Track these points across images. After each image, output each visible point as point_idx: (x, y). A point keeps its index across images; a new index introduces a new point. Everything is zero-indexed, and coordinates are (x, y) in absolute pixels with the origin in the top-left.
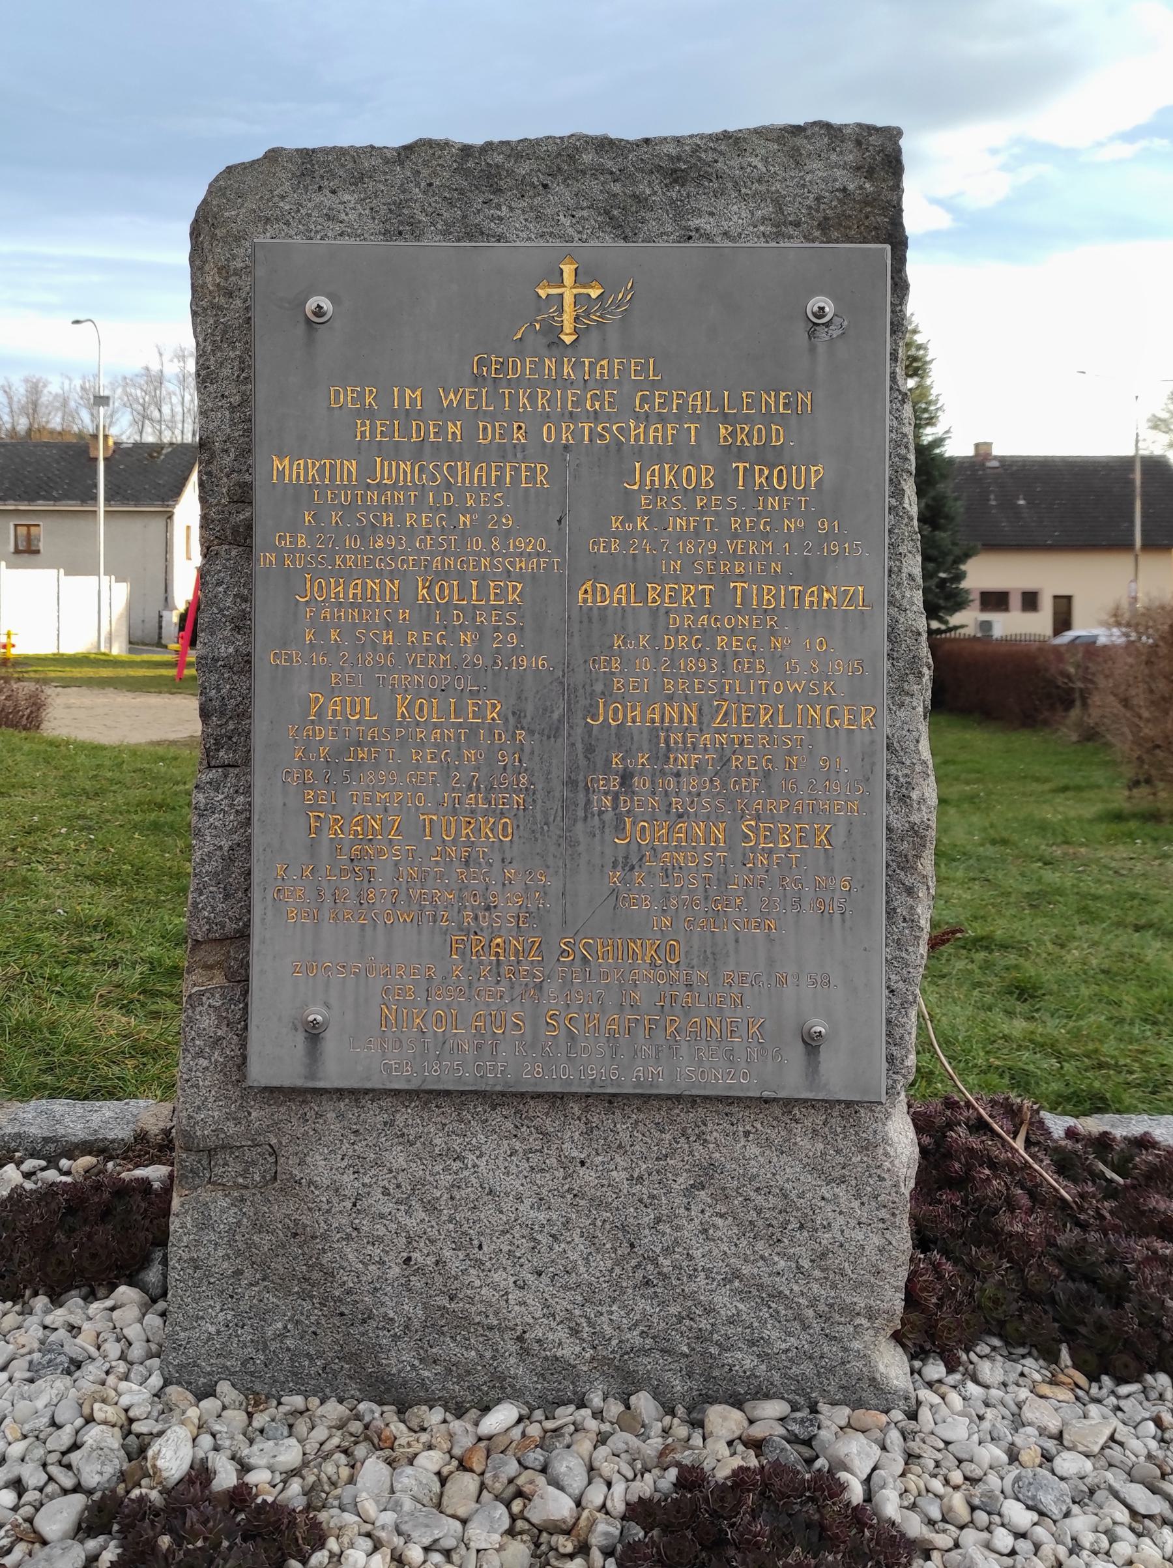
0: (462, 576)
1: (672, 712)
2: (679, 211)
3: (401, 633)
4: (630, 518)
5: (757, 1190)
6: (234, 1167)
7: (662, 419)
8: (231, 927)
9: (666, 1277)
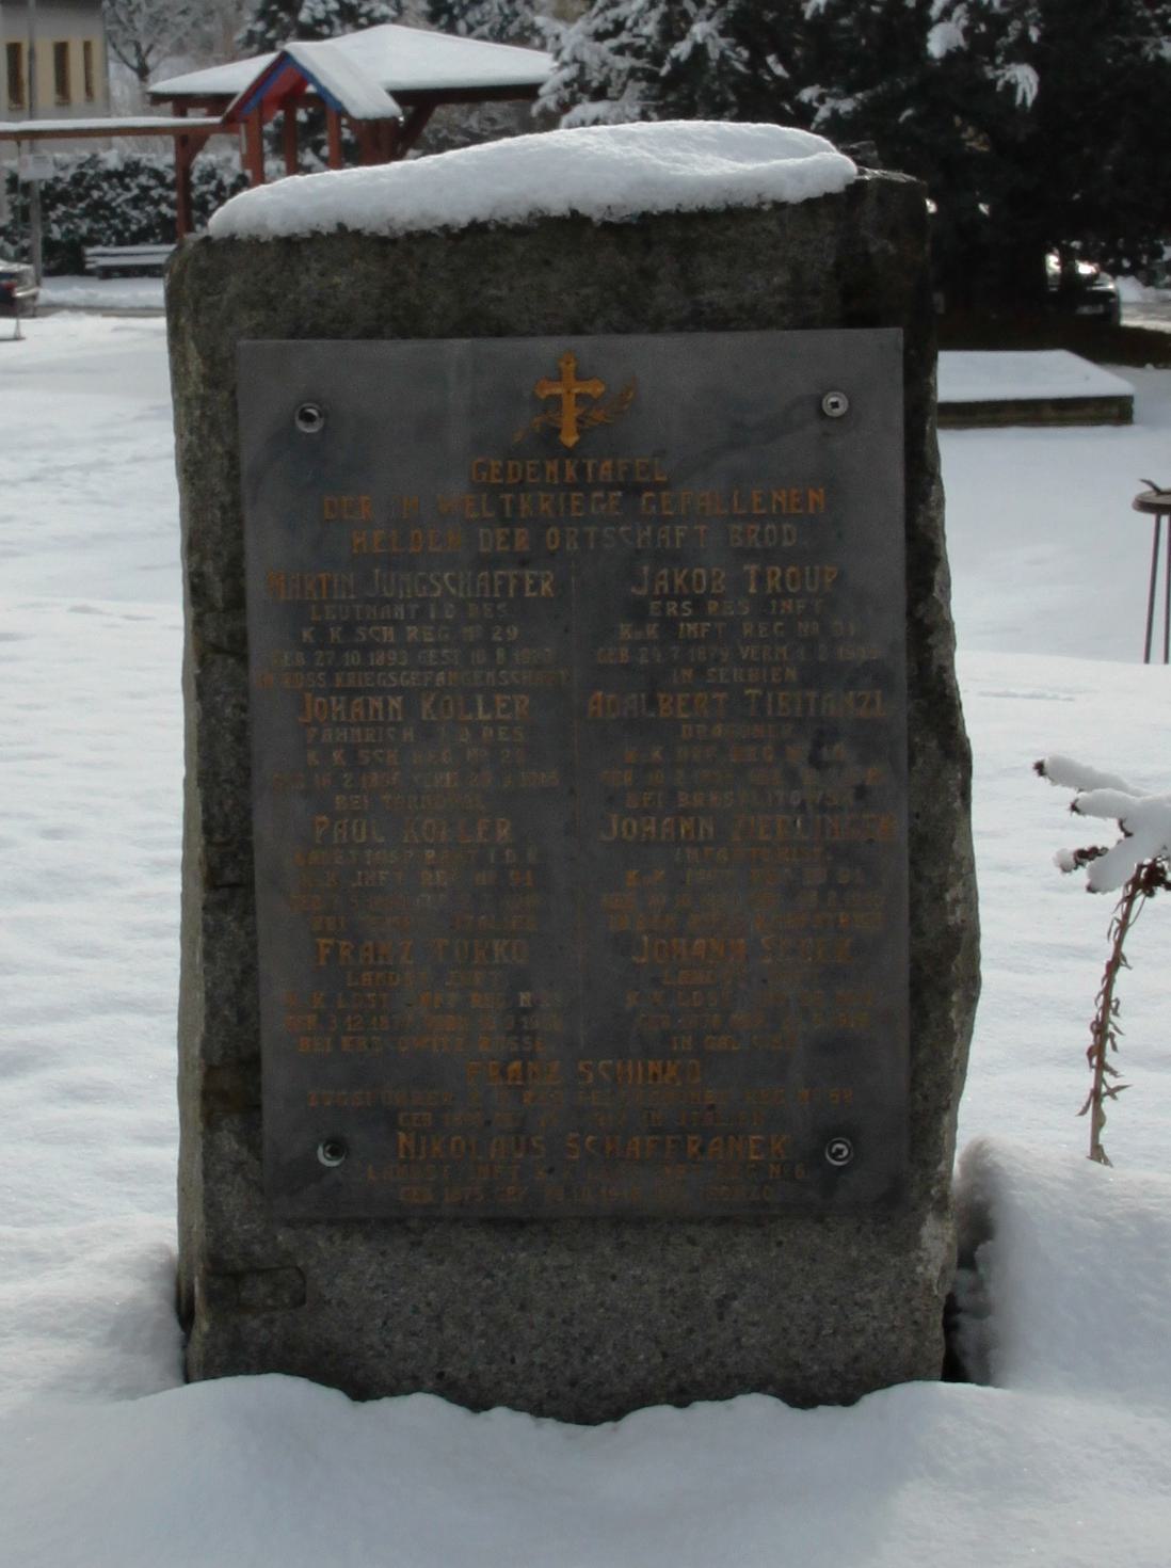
5: (790, 1297)
6: (263, 1289)
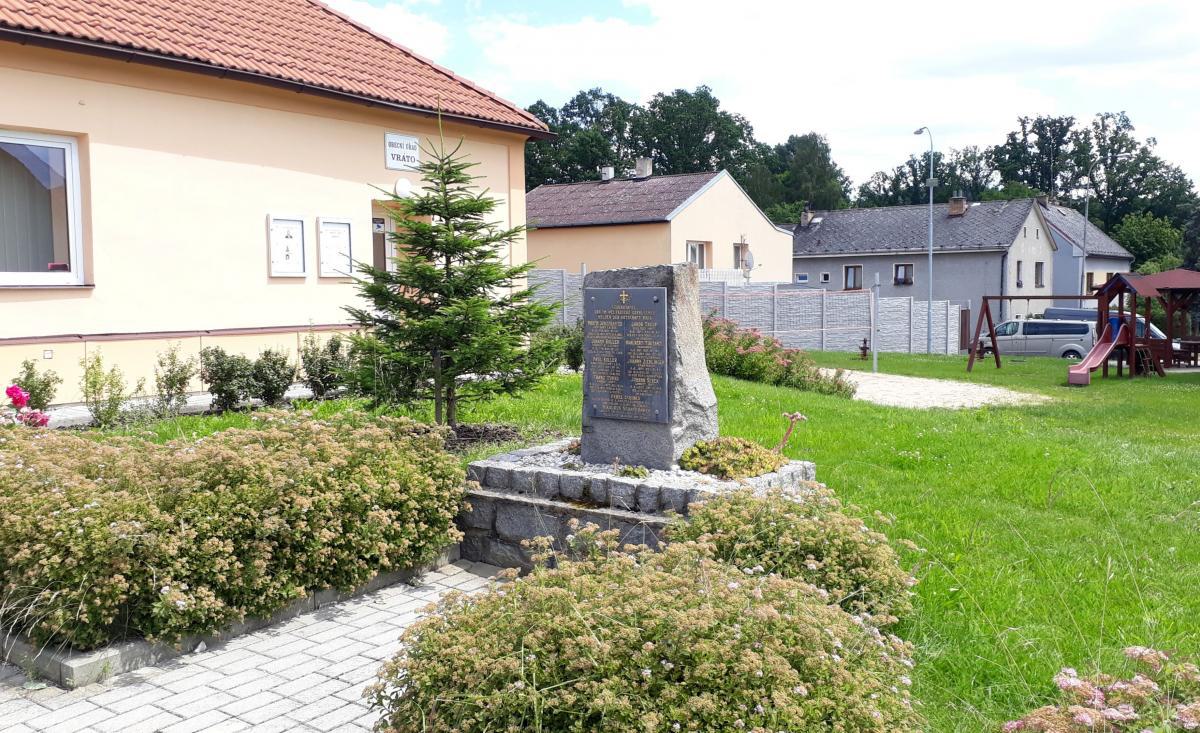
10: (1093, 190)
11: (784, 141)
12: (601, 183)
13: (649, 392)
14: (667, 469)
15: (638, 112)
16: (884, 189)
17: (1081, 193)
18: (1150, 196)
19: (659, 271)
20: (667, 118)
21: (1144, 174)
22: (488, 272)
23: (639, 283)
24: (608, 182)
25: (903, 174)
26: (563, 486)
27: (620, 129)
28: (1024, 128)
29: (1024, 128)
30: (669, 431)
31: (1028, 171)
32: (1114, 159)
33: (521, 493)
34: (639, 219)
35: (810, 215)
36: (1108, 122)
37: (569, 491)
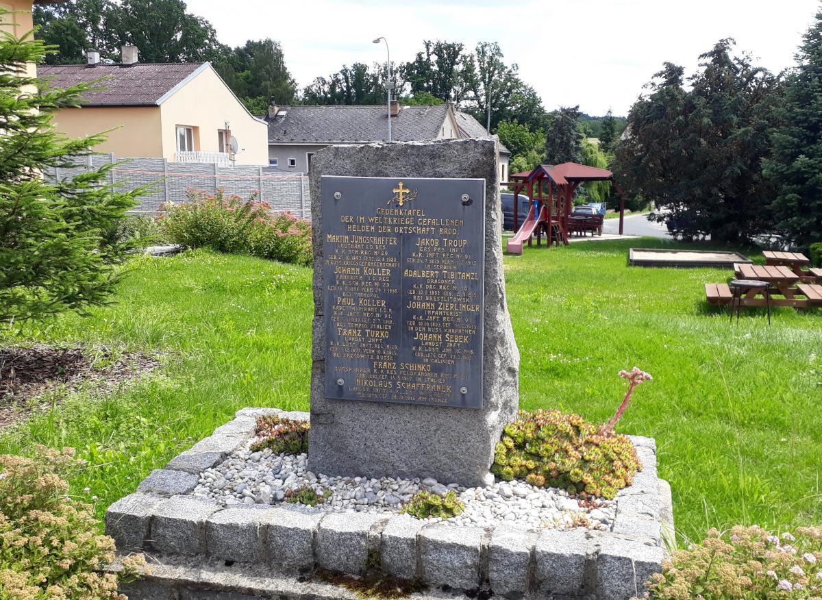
0: (376, 268)
1: (428, 305)
2: (434, 166)
3: (360, 283)
4: (417, 254)
7: (426, 227)
8: (322, 358)
9: (429, 452)
10: (476, 102)
11: (242, 45)
12: (87, 67)
13: (448, 357)
14: (478, 483)
15: (110, 7)
16: (324, 92)
17: (468, 103)
18: (514, 108)
19: (466, 150)
20: (139, 16)
21: (510, 91)
22: (45, 146)
23: (427, 169)
24: (93, 66)
25: (338, 81)
26: (323, 553)
27: (95, 21)
28: (428, 49)
29: (428, 49)
30: (482, 421)
31: (431, 84)
32: (490, 78)
33: (229, 563)
34: (128, 103)
35: (276, 109)
36: (487, 48)
37: (334, 559)
